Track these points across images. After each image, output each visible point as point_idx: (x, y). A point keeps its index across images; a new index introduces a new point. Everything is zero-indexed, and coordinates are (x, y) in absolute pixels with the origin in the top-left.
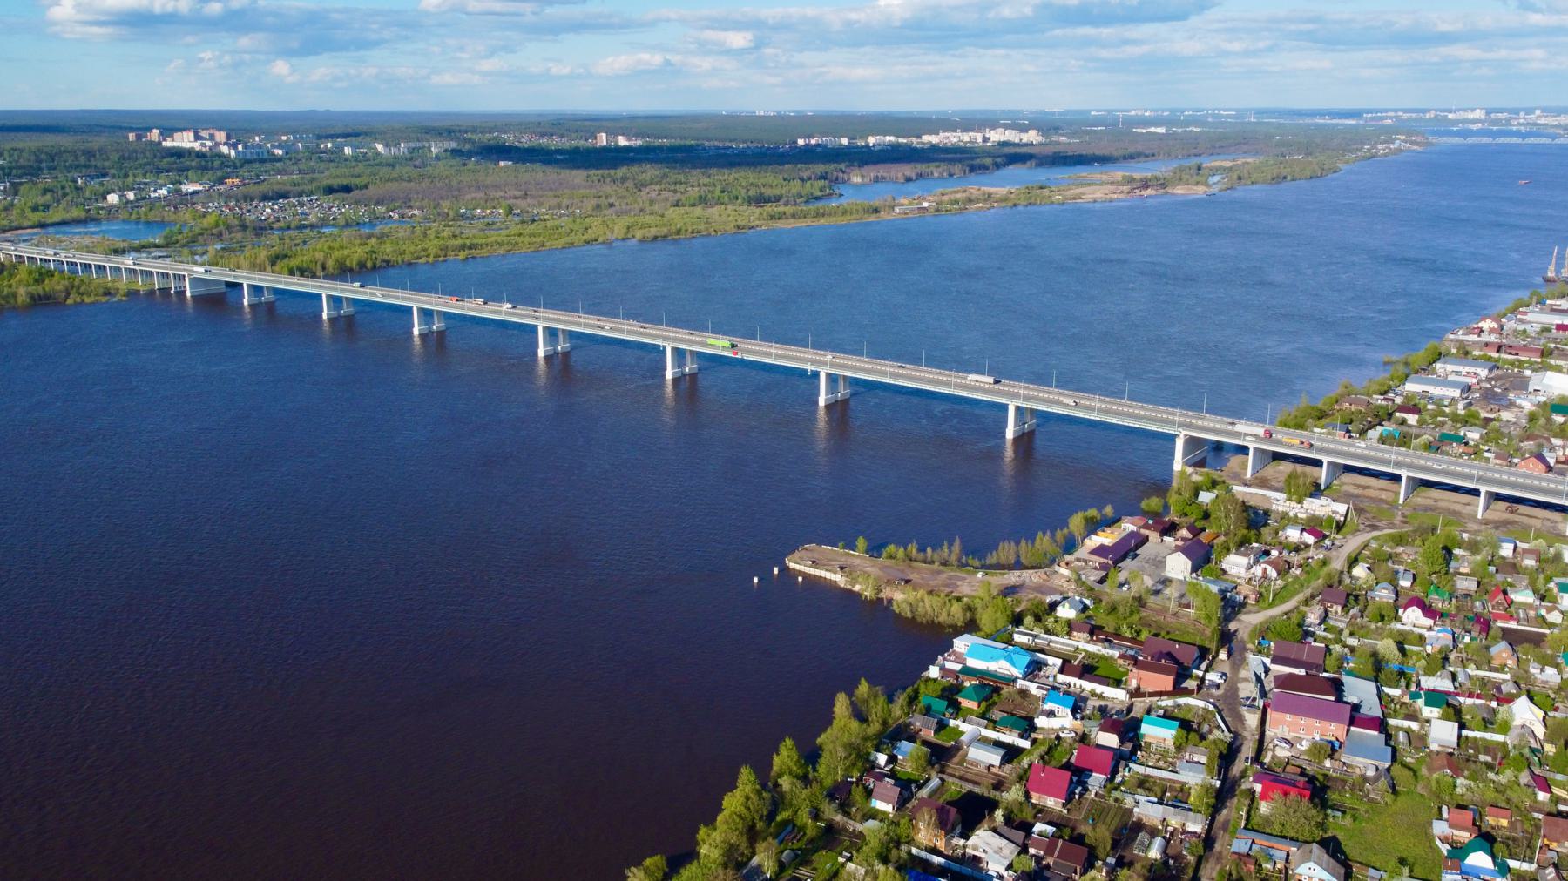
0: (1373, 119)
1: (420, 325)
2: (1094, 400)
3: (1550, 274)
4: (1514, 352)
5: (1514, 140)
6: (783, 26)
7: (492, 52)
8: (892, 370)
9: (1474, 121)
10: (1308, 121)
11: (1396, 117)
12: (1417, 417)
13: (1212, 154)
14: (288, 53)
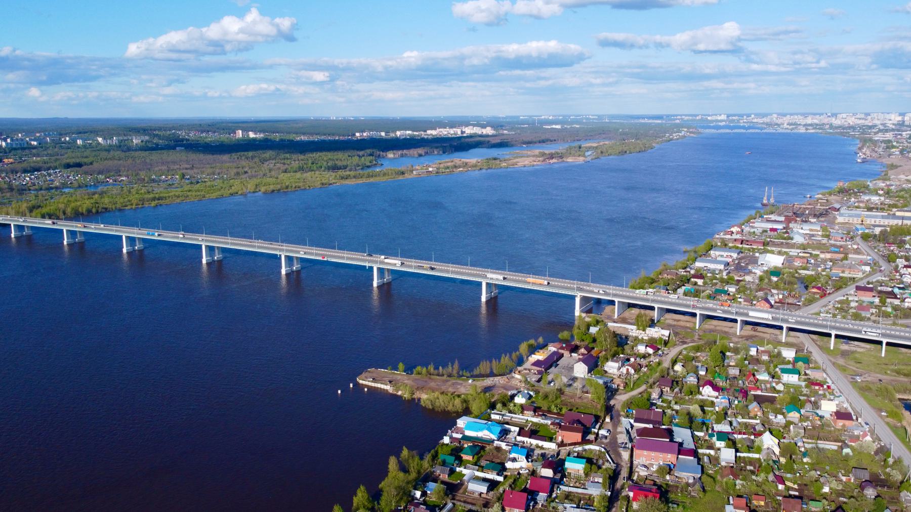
1: (127, 246)
3: (765, 202)
6: (348, 69)
7: (169, 84)
9: (721, 121)
10: (636, 121)
12: (702, 280)
14: (39, 83)
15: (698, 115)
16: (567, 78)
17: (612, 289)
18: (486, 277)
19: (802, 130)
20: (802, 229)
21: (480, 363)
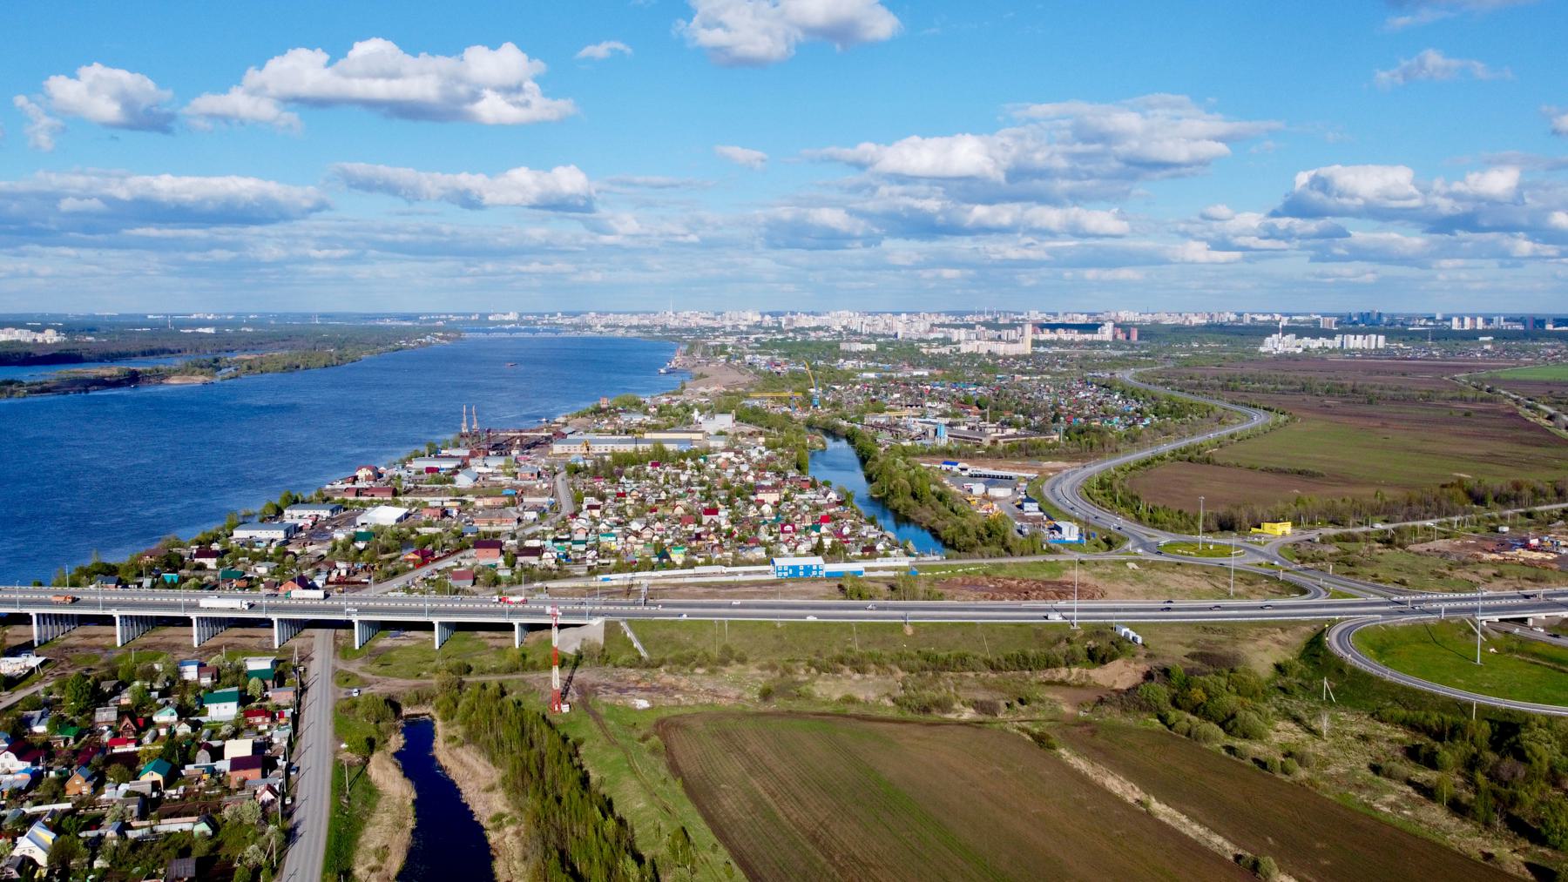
0: (426, 321)
2: (14, 592)
3: (465, 430)
4: (370, 494)
5: (504, 335)
8: (21, 596)
9: (509, 322)
10: (370, 323)
11: (447, 320)
12: (215, 560)
13: (246, 350)
15: (474, 314)
16: (267, 244)
17: (32, 593)
18: (196, 607)
19: (620, 333)
20: (486, 465)
21: (20, 757)
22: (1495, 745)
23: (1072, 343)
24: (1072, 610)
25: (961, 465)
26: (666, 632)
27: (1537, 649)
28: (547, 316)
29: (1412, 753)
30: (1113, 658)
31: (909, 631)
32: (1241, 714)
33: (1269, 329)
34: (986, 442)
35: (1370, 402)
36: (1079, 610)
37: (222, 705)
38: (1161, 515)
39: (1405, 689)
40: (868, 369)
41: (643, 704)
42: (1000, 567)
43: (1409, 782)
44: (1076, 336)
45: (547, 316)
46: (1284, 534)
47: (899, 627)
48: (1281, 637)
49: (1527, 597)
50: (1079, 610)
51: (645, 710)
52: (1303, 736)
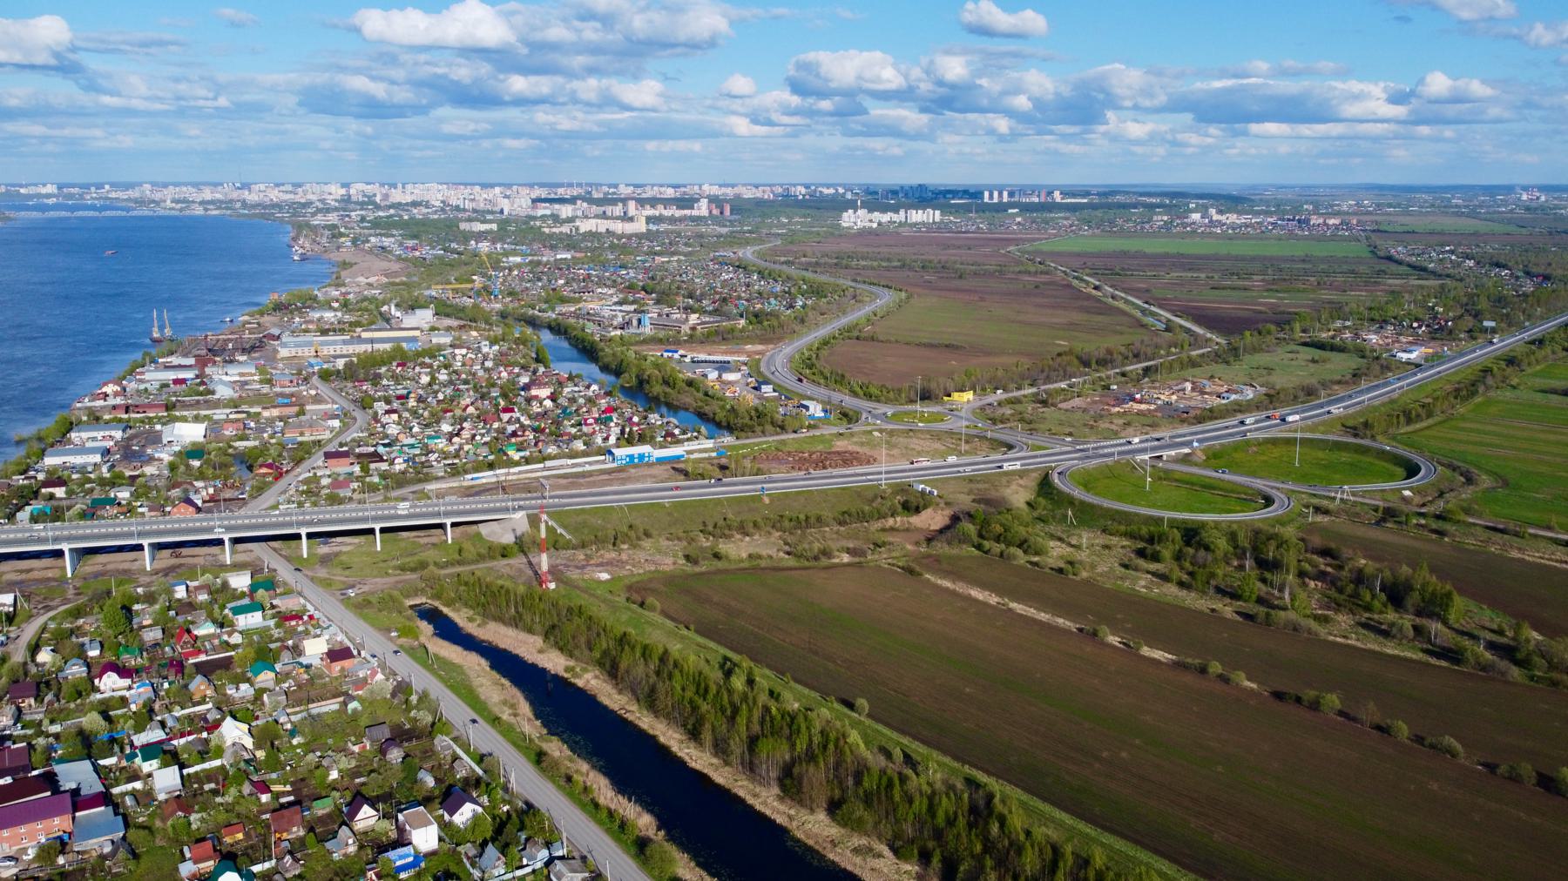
3: (156, 335)
9: (48, 196)
12: (64, 489)
22: (1188, 543)
23: (672, 220)
24: (880, 473)
25: (681, 352)
26: (580, 519)
27: (1177, 477)
28: (93, 189)
29: (1141, 553)
30: (925, 507)
31: (767, 500)
32: (1032, 539)
33: (841, 204)
34: (685, 329)
35: (960, 277)
36: (886, 473)
37: (249, 615)
38: (874, 391)
39: (1117, 512)
40: (514, 253)
41: (605, 576)
42: (783, 442)
43: (1148, 572)
44: (673, 212)
45: (93, 189)
46: (968, 401)
47: (758, 499)
48: (1021, 482)
49: (1158, 440)
50: (886, 473)
51: (607, 581)
52: (1069, 549)
